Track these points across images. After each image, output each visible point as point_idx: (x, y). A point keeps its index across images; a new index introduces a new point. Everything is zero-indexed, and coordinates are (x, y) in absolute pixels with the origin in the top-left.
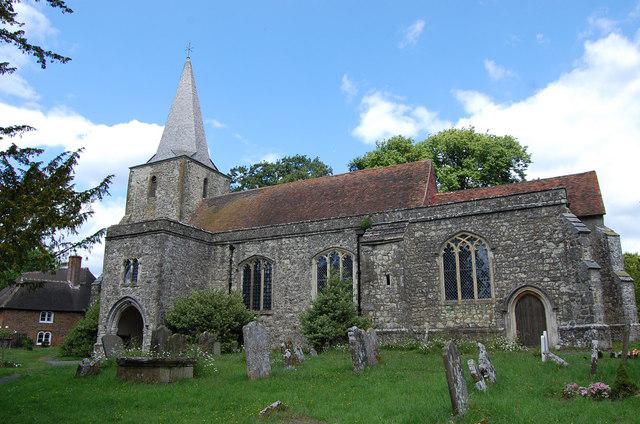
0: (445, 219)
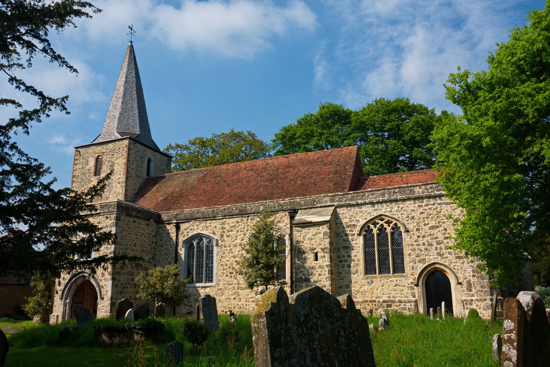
0: (365, 204)
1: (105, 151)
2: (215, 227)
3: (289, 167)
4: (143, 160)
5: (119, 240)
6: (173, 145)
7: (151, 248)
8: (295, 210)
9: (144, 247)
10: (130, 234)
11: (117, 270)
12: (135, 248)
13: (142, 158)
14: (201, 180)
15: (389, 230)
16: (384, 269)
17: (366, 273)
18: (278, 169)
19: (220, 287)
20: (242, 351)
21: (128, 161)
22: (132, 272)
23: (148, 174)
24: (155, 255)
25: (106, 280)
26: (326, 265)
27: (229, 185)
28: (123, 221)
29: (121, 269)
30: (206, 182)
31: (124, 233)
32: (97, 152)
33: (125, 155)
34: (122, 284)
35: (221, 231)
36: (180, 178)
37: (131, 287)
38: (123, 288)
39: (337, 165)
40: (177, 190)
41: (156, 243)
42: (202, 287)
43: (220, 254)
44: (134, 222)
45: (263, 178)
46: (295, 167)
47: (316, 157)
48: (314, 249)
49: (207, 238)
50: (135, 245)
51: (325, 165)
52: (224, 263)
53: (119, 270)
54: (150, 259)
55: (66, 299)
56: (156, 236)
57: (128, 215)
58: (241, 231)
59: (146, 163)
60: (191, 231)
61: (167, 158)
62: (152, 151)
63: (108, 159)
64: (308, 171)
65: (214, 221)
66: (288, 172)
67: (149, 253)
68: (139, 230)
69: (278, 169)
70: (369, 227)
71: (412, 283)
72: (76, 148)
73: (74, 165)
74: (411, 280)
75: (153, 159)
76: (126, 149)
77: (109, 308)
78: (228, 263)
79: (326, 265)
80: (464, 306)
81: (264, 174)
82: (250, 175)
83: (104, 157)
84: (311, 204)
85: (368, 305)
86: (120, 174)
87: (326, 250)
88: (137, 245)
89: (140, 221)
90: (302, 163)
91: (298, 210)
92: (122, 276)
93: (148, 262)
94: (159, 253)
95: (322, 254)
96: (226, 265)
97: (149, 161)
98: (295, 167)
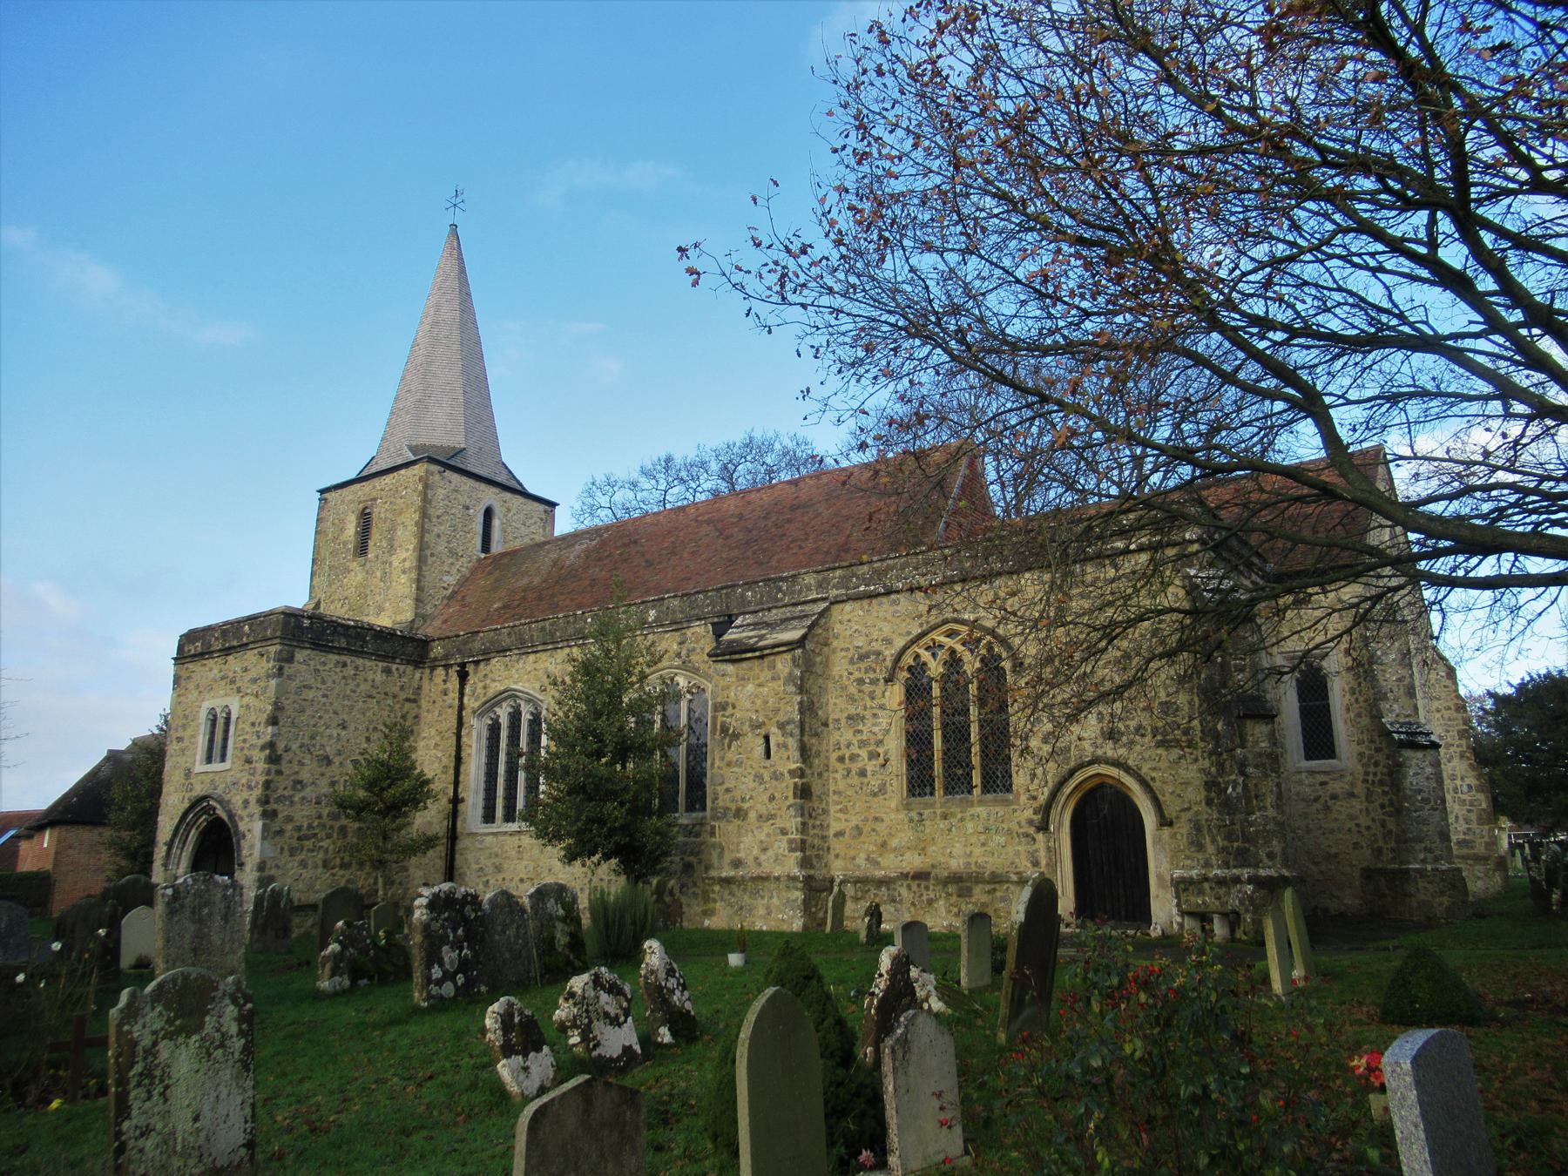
3: (794, 508)
6: (601, 479)
8: (730, 616)
15: (971, 664)
16: (957, 783)
17: (912, 791)
23: (486, 546)
26: (790, 772)
34: (299, 828)
48: (759, 726)
49: (528, 701)
59: (480, 518)
61: (542, 507)
62: (496, 490)
70: (917, 656)
71: (1030, 822)
72: (322, 492)
74: (1029, 813)
75: (498, 511)
79: (790, 772)
80: (1178, 897)
85: (909, 887)
87: (789, 728)
89: (360, 661)
91: (737, 616)
95: (781, 740)
97: (488, 514)
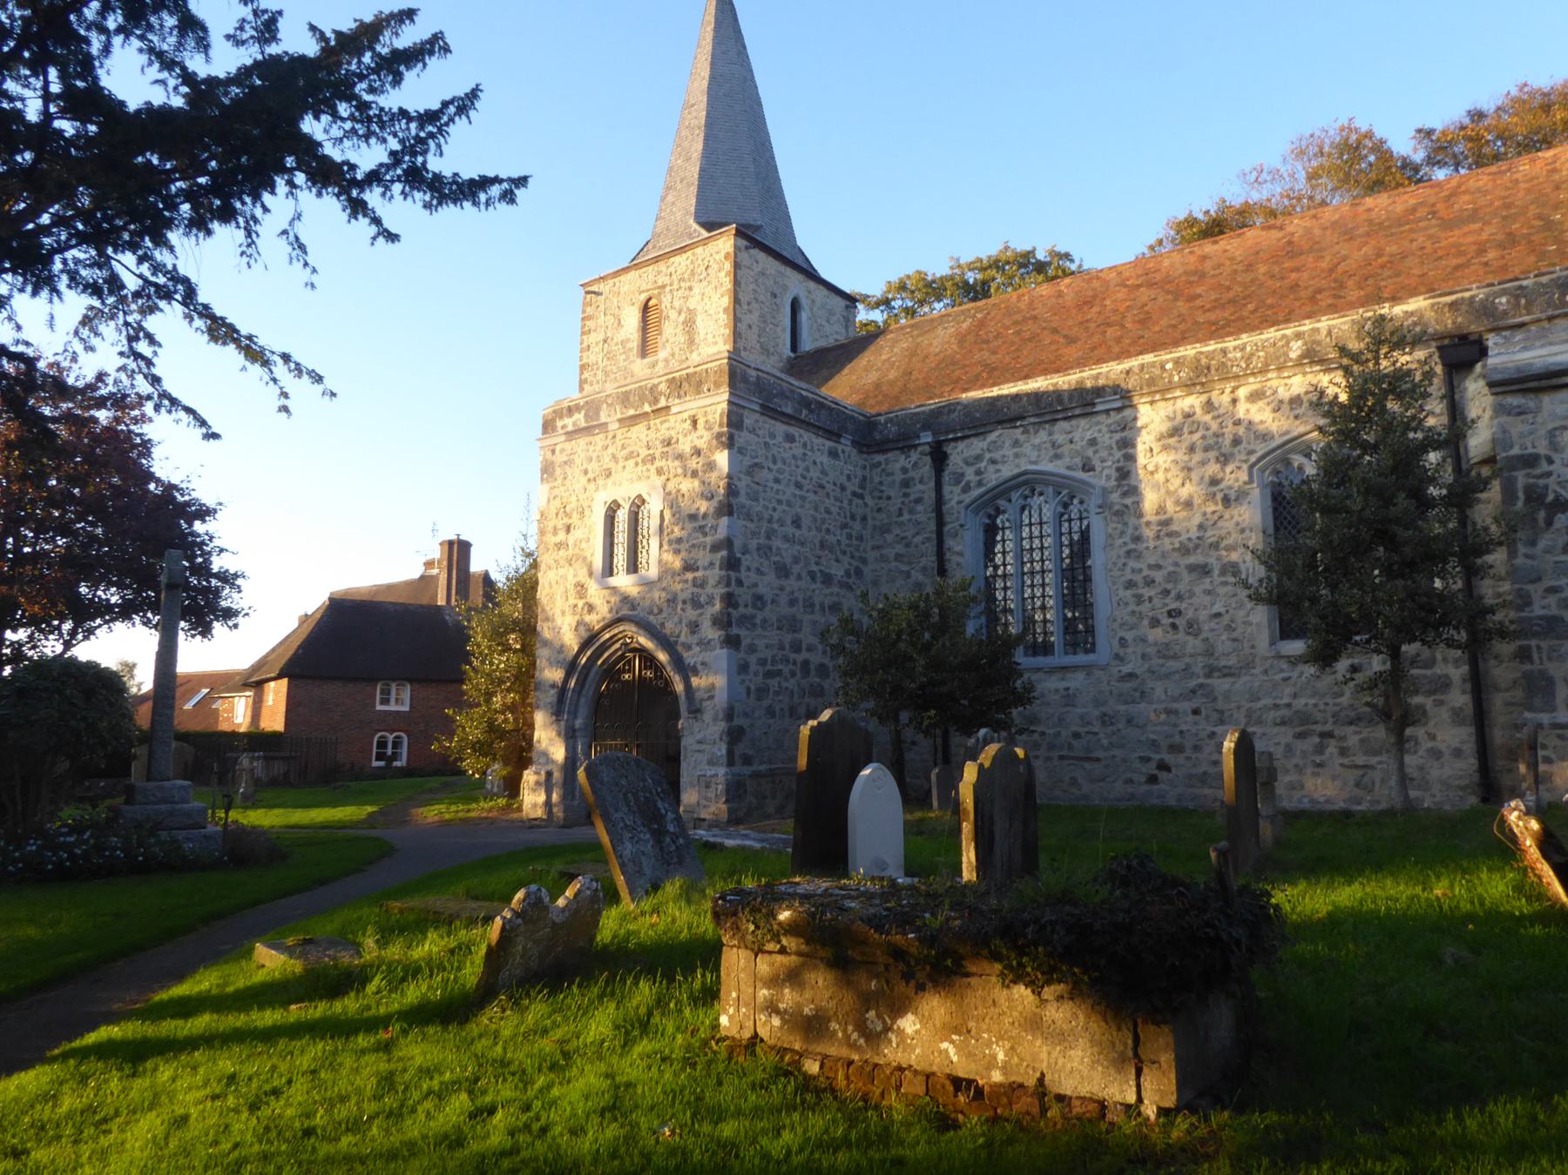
1: (667, 280)
2: (1093, 442)
4: (778, 301)
5: (742, 499)
7: (849, 537)
9: (828, 531)
10: (777, 481)
11: (742, 610)
12: (798, 533)
13: (775, 296)
14: (971, 338)
18: (1250, 267)
19: (1126, 669)
20: (229, 609)
21: (736, 301)
22: (794, 618)
23: (794, 348)
24: (864, 561)
25: (705, 644)
27: (1071, 341)
28: (753, 431)
29: (754, 606)
30: (987, 342)
31: (764, 475)
32: (644, 287)
33: (727, 283)
34: (763, 662)
35: (1118, 454)
36: (896, 341)
37: (793, 674)
38: (769, 675)
39: (1505, 218)
40: (892, 375)
41: (864, 519)
42: (1052, 670)
43: (1119, 542)
44: (790, 438)
45: (1198, 302)
46: (1321, 250)
47: (1399, 208)
50: (797, 523)
51: (1448, 225)
52: (1138, 578)
53: (750, 611)
54: (848, 574)
55: (574, 714)
56: (861, 497)
57: (769, 411)
58: (1206, 449)
60: (991, 468)
61: (842, 303)
63: (677, 304)
64: (1379, 255)
65: (1083, 422)
66: (1297, 270)
67: (844, 553)
68: (807, 469)
69: (1250, 267)
73: (583, 333)
75: (804, 302)
76: (728, 266)
77: (722, 750)
78: (1159, 576)
81: (1199, 290)
82: (1145, 299)
83: (666, 300)
84: (1550, 303)
86: (716, 343)
88: (806, 522)
89: (807, 436)
90: (1348, 235)
92: (759, 631)
93: (843, 585)
94: (876, 553)
96: (1150, 582)
97: (795, 306)
98: (1321, 250)
